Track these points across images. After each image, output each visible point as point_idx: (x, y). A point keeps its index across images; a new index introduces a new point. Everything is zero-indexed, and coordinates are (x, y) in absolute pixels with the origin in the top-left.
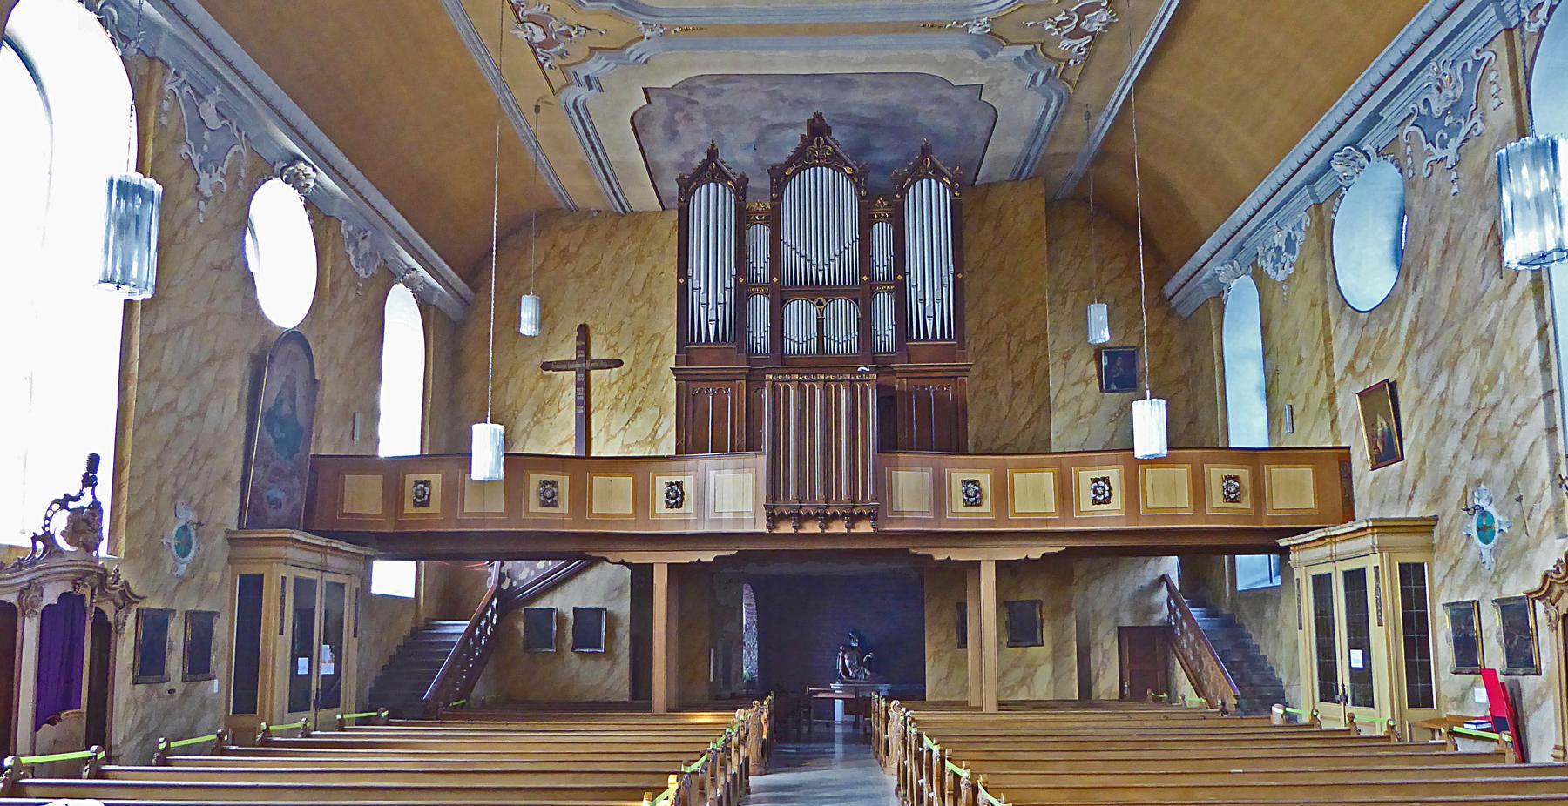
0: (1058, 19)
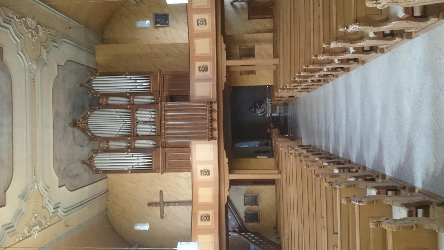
0: (30, 36)
